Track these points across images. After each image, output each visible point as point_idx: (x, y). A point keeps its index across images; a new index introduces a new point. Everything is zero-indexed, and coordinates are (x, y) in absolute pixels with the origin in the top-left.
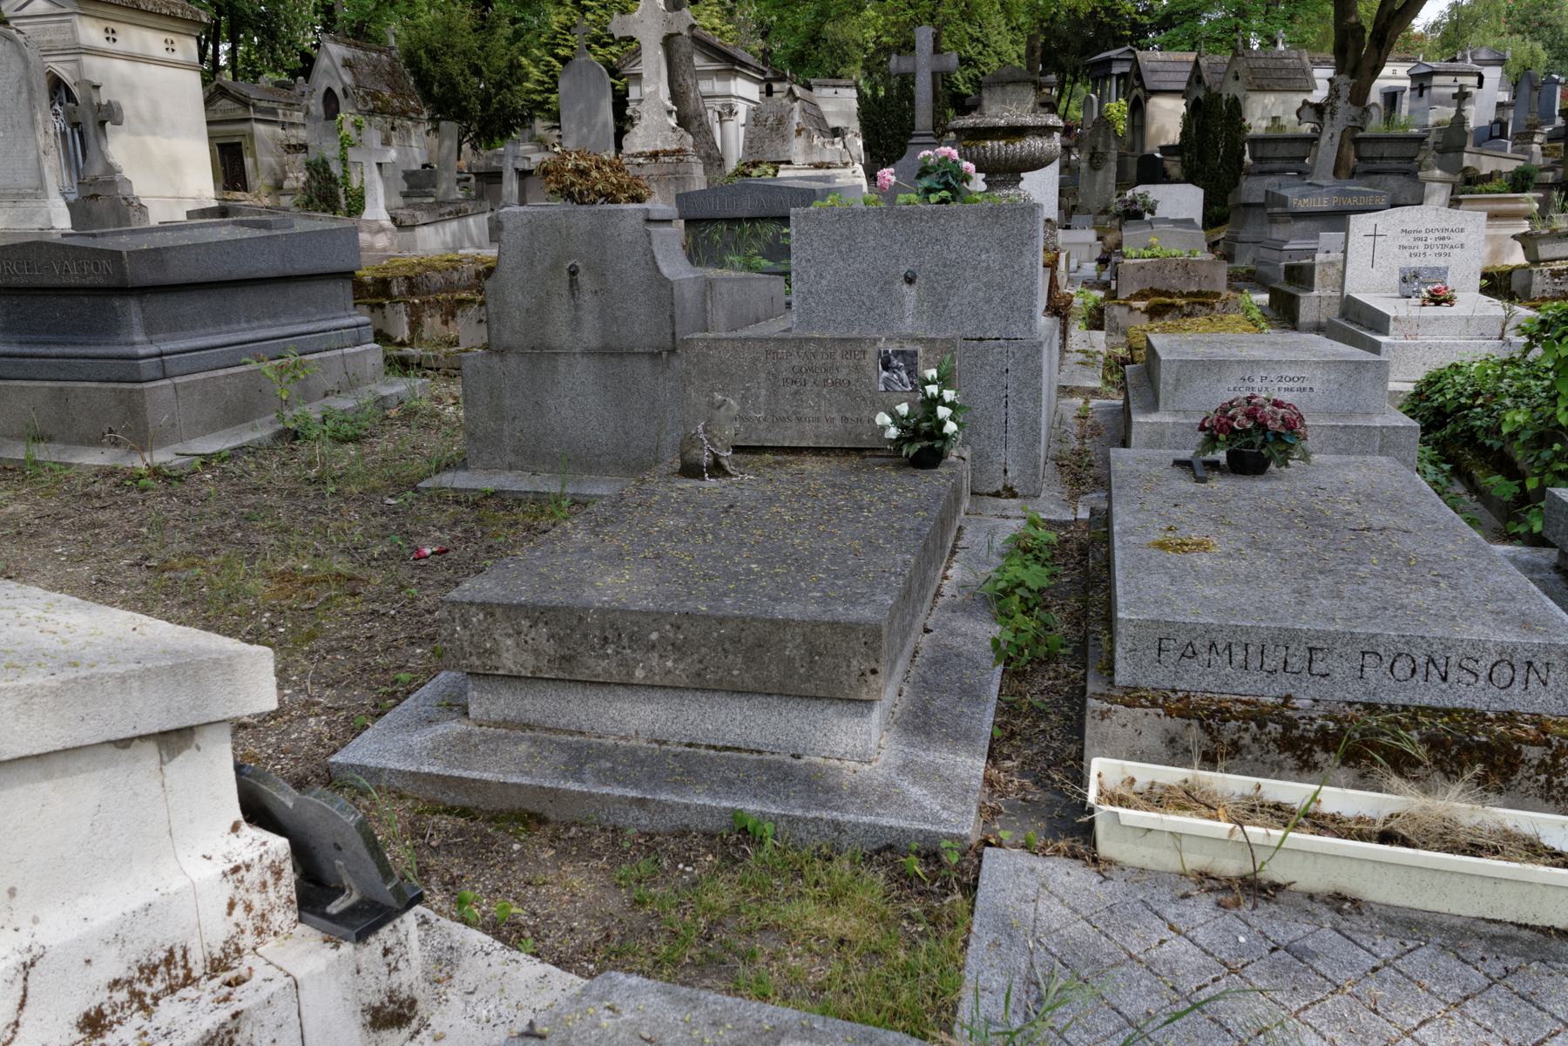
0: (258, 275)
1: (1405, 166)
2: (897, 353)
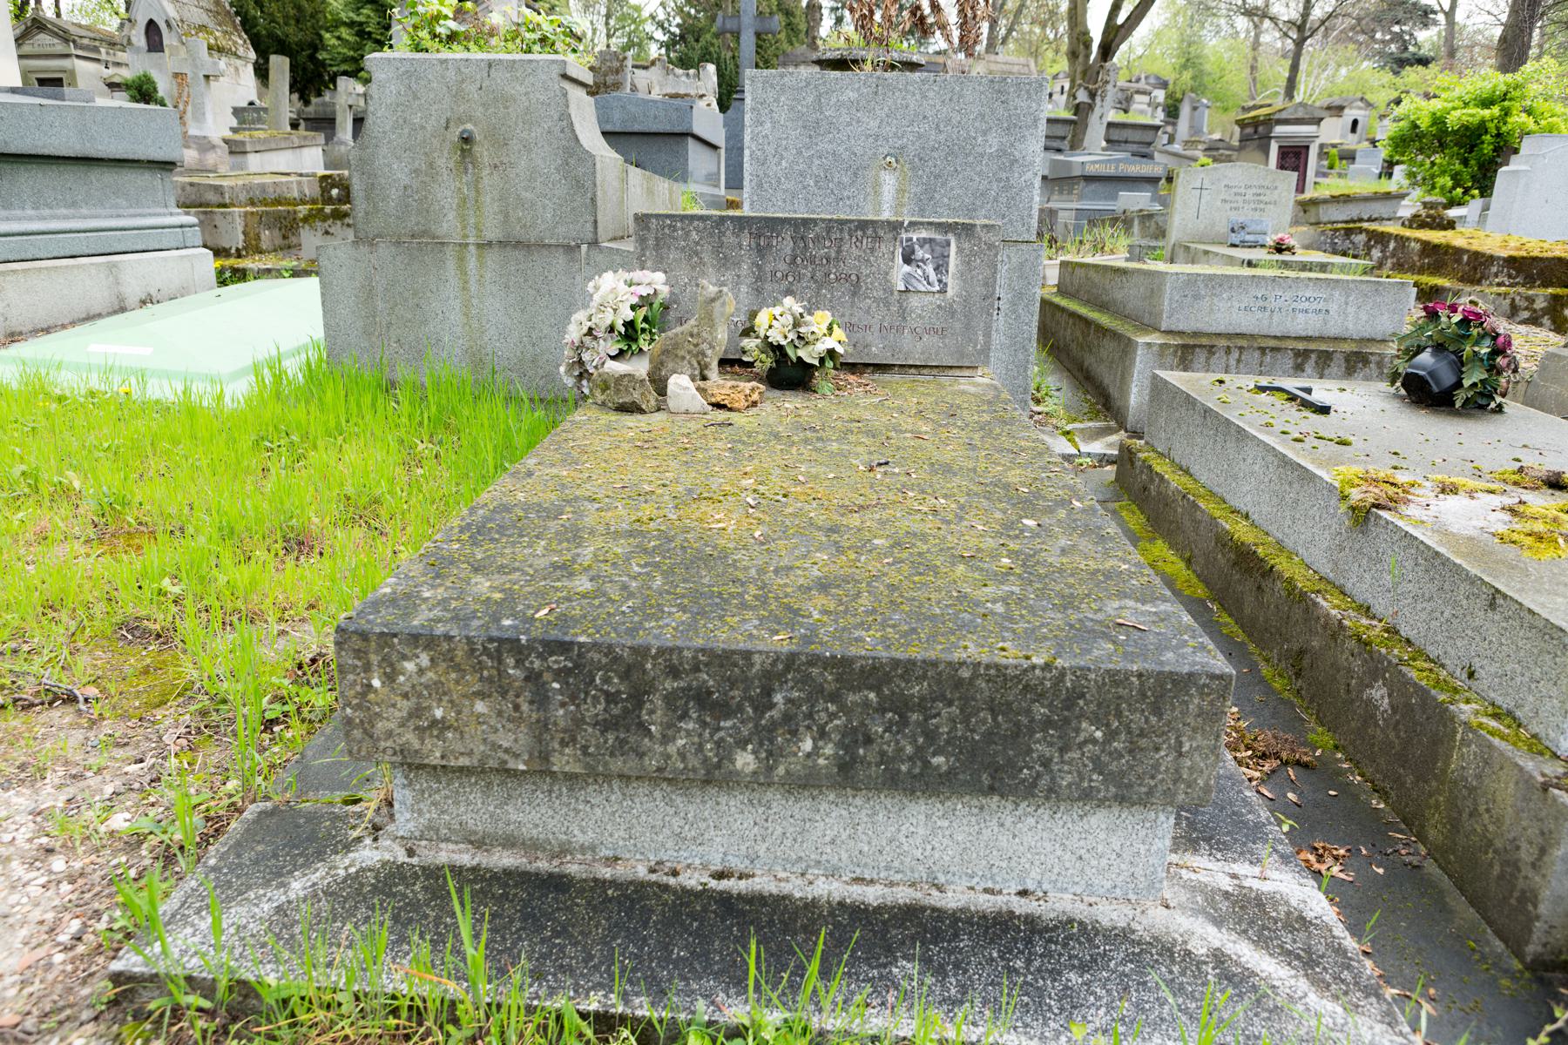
0: (46, 152)
1: (1144, 150)
2: (923, 242)
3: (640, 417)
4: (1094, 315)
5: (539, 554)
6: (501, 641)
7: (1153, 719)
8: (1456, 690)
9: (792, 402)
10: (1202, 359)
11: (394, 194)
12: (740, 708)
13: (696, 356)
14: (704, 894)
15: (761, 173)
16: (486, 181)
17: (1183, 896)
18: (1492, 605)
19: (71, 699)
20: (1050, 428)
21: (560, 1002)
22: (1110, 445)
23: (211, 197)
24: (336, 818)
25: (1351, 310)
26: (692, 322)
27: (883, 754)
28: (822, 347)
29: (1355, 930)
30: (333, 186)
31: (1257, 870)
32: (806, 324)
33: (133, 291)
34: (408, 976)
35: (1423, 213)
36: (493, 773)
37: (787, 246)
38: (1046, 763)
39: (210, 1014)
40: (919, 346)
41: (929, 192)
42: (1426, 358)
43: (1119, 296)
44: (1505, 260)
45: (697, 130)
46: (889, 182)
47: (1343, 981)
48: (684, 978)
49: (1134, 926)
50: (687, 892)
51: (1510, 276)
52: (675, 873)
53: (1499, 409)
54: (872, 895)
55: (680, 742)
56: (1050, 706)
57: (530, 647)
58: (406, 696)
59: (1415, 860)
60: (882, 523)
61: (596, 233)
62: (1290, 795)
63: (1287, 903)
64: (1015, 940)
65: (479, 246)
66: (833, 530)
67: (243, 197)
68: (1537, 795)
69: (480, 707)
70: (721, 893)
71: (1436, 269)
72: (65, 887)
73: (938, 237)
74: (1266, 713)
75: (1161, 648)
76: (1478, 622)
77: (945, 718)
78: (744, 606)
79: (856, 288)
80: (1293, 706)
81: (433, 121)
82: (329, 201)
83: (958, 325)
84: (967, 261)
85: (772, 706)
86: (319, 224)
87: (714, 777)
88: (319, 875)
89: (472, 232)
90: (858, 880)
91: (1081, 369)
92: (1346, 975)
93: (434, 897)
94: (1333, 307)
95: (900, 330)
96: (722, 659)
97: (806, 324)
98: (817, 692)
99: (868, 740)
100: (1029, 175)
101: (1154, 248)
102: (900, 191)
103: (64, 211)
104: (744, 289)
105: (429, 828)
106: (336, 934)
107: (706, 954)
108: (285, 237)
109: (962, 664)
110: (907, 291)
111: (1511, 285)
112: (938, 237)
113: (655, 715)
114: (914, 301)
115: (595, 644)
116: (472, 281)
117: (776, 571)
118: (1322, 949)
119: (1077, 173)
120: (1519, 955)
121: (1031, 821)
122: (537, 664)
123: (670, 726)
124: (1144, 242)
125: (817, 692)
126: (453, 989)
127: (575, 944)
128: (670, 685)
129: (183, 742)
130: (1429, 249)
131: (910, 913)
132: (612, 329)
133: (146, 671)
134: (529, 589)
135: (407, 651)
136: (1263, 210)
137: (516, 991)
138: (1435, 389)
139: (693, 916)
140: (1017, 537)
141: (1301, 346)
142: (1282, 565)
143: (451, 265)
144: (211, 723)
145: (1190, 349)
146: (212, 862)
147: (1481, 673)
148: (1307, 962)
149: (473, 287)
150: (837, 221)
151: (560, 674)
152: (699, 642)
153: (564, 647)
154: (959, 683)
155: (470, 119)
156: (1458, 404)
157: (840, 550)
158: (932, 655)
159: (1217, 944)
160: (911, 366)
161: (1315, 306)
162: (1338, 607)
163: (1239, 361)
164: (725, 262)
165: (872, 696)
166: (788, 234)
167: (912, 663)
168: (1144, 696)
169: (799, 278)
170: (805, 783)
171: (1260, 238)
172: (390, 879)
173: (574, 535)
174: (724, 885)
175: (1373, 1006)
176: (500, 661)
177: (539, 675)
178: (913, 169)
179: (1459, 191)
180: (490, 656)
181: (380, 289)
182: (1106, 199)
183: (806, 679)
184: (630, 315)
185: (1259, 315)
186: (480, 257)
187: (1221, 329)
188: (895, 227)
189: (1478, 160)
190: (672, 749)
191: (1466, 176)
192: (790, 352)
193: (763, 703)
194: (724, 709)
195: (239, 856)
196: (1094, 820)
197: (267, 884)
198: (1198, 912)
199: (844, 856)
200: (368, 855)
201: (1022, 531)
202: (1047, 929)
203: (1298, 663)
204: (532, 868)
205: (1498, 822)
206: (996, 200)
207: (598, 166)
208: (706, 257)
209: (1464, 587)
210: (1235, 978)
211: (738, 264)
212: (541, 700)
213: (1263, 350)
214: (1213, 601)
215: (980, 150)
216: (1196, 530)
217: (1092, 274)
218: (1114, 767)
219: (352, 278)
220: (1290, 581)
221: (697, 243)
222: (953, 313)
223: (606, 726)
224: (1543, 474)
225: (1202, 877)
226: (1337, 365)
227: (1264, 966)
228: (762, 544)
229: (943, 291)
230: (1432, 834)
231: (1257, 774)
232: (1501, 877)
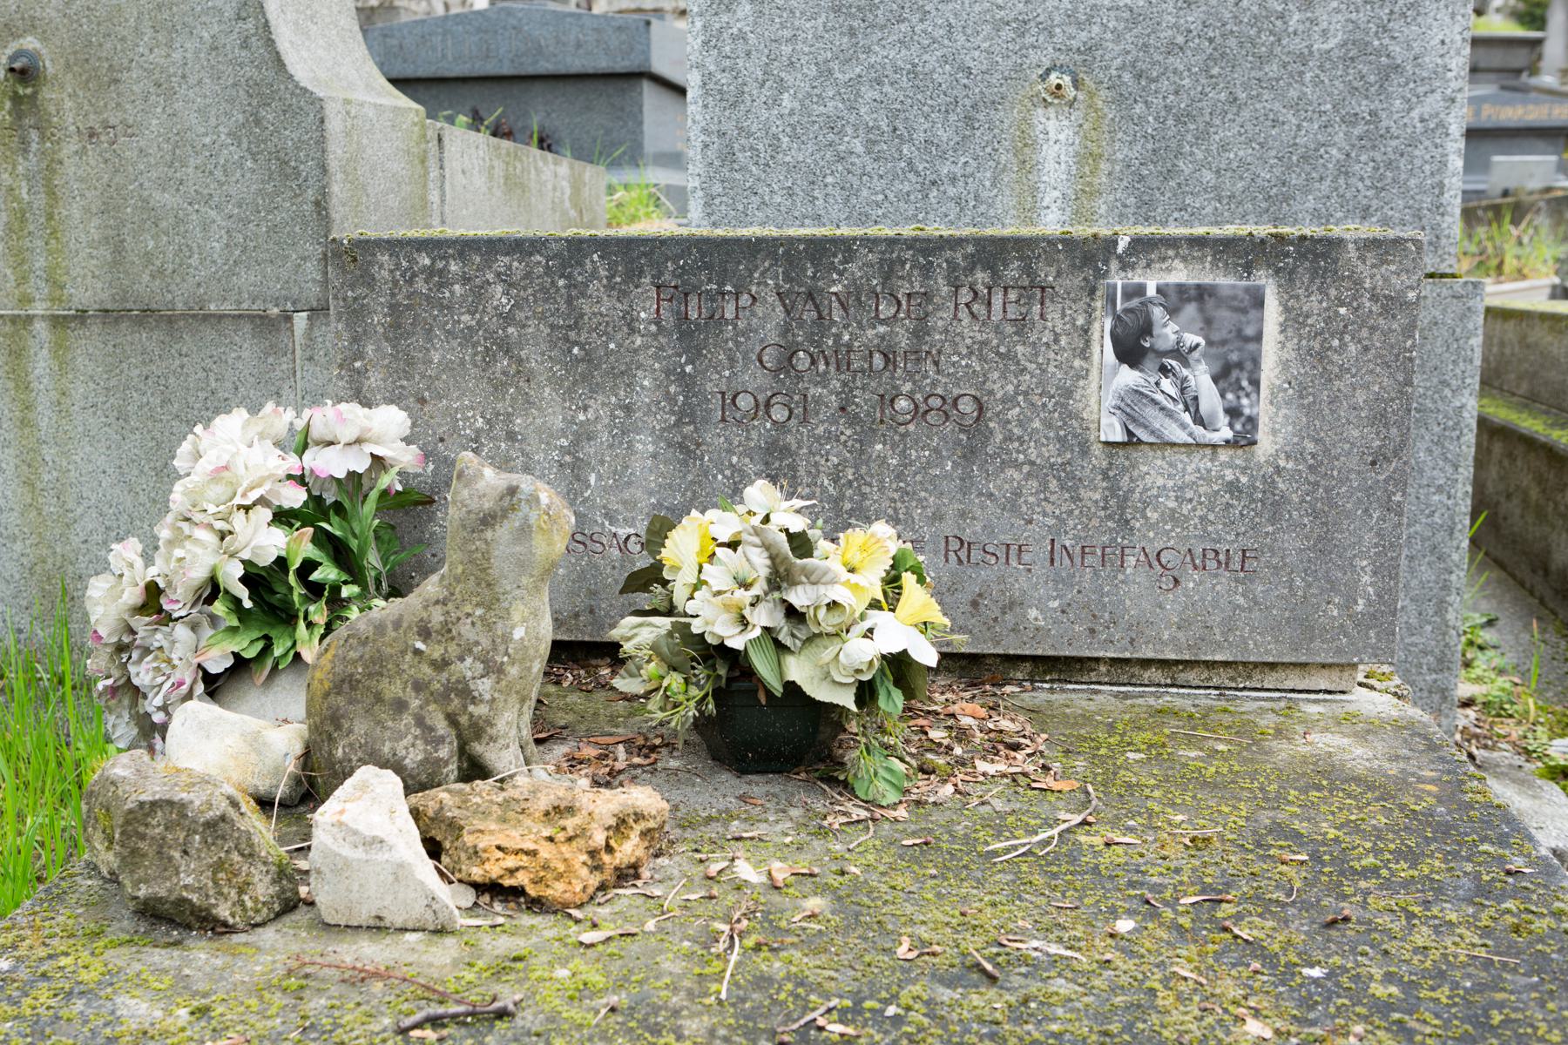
2: (1177, 298)
3: (201, 955)
9: (767, 845)
13: (443, 697)
15: (728, 127)
16: (70, 168)
20: (1504, 755)
26: (431, 587)
28: (861, 652)
32: (814, 578)
37: (768, 320)
40: (1173, 604)
41: (1164, 155)
45: (660, 66)
46: (1057, 136)
65: (57, 322)
73: (1224, 281)
79: (974, 437)
83: (1291, 543)
84: (1316, 355)
89: (38, 287)
95: (1113, 557)
97: (814, 578)
100: (1433, 103)
102: (1087, 158)
104: (644, 444)
110: (1132, 442)
112: (1224, 281)
114: (1153, 473)
132: (212, 590)
149: (45, 418)
150: (911, 243)
155: (32, 27)
160: (1146, 663)
164: (587, 370)
166: (767, 284)
169: (805, 411)
178: (1121, 100)
186: (58, 348)
188: (1089, 255)
192: (762, 665)
206: (1343, 171)
207: (334, 125)
208: (534, 356)
211: (624, 375)
215: (1297, 45)
217: (1539, 334)
221: (508, 319)
222: (1275, 507)
229: (1244, 441)
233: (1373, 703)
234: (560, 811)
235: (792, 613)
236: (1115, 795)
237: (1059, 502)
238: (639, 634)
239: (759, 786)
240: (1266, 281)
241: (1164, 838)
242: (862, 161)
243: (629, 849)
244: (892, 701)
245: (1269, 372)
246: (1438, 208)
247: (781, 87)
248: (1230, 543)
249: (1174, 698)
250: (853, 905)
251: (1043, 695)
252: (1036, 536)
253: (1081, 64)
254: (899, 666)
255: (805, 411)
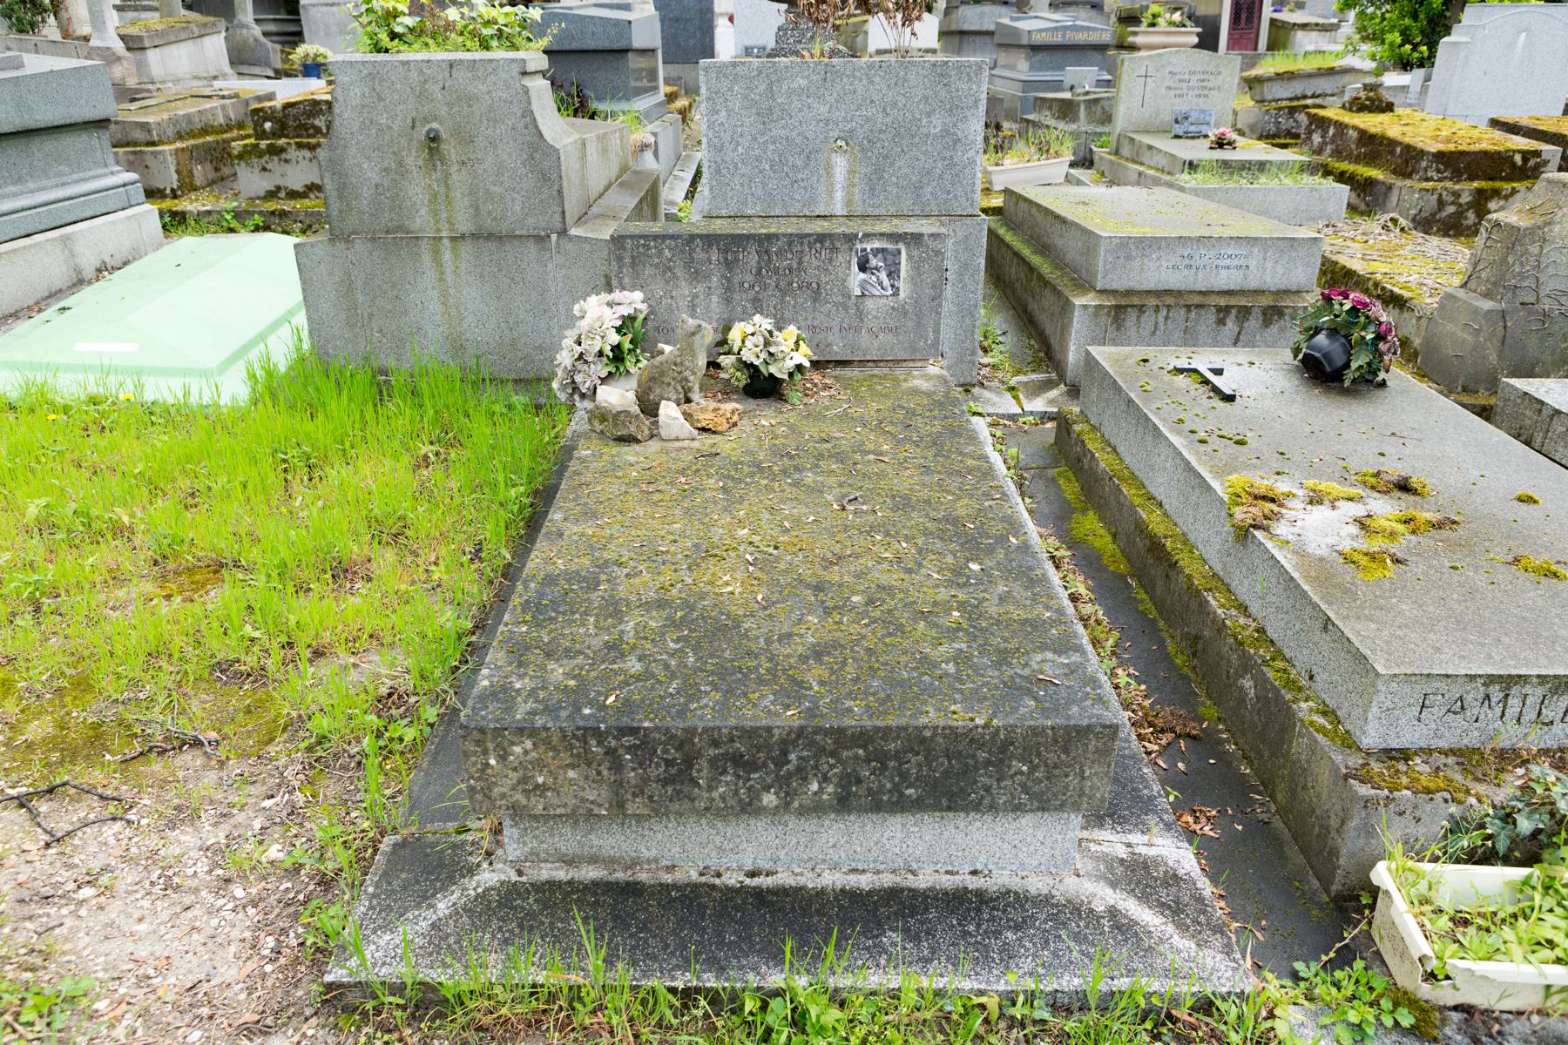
2: (876, 252)
3: (637, 447)
4: (1036, 260)
5: (589, 633)
6: (586, 729)
7: (1063, 757)
8: (1300, 689)
9: (767, 416)
10: (1134, 318)
11: (366, 192)
12: (765, 765)
14: (742, 889)
17: (1090, 866)
18: (1325, 629)
19: (197, 743)
21: (654, 982)
22: (1051, 402)
23: (138, 135)
24: (454, 846)
25: (1269, 264)
27: (869, 789)
28: (790, 364)
29: (1214, 881)
30: (266, 119)
31: (1146, 838)
32: (776, 344)
33: (88, 264)
34: (538, 969)
35: (1363, 95)
36: (582, 817)
37: (753, 259)
38: (988, 789)
39: (404, 1008)
40: (876, 344)
42: (1321, 339)
43: (1059, 242)
44: (1434, 155)
46: (840, 164)
47: (1199, 923)
48: (736, 957)
49: (1054, 892)
50: (729, 889)
51: (1438, 171)
52: (719, 875)
53: (1383, 384)
54: (864, 882)
55: (721, 790)
56: (989, 752)
57: (608, 732)
58: (515, 769)
59: (1264, 817)
60: (858, 576)
61: (564, 222)
62: (1180, 765)
63: (1166, 864)
64: (969, 910)
65: (453, 239)
66: (818, 588)
67: (170, 132)
68: (1341, 782)
69: (571, 774)
70: (754, 888)
71: (1371, 159)
72: (251, 911)
73: (890, 246)
74: (1168, 689)
75: (1070, 702)
76: (1316, 639)
77: (913, 764)
78: (760, 681)
79: (816, 296)
80: (1190, 681)
81: (398, 122)
82: (261, 135)
83: (910, 324)
85: (788, 762)
86: (255, 160)
87: (749, 808)
88: (455, 896)
90: (854, 871)
91: (1025, 311)
92: (1202, 918)
93: (545, 907)
94: (1253, 263)
95: (858, 330)
96: (751, 733)
97: (776, 344)
98: (821, 751)
99: (859, 781)
100: (972, 153)
101: (1100, 134)
102: (851, 172)
103: (12, 189)
104: (715, 299)
105: (532, 854)
106: (480, 942)
107: (749, 937)
108: (217, 170)
109: (925, 727)
110: (863, 295)
111: (1440, 180)
113: (702, 772)
114: (870, 304)
115: (656, 728)
116: (448, 272)
117: (779, 640)
118: (1187, 899)
119: (1025, 42)
120: (1327, 891)
121: (979, 824)
122: (613, 743)
123: (713, 779)
124: (1090, 128)
125: (821, 751)
126: (575, 978)
127: (655, 937)
128: (712, 752)
129: (301, 777)
130: (1366, 138)
131: (893, 893)
132: (601, 354)
133: (248, 711)
134: (593, 674)
135: (515, 739)
136: (1206, 96)
137: (623, 974)
138: (1328, 369)
139: (737, 908)
140: (964, 585)
141: (1222, 302)
142: (1184, 561)
143: (427, 257)
144: (323, 757)
145: (1124, 309)
146: (371, 890)
147: (1317, 678)
148: (1174, 911)
149: (449, 278)
151: (629, 749)
152: (733, 722)
153: (634, 731)
154: (923, 740)
155: (435, 119)
156: (1347, 384)
157: (827, 612)
158: (903, 721)
159: (1112, 902)
161: (1236, 262)
162: (1223, 606)
163: (1167, 318)
164: (696, 276)
165: (860, 751)
166: (753, 248)
167: (889, 728)
168: (1056, 741)
169: (765, 287)
170: (816, 809)
171: (1204, 129)
172: (509, 895)
173: (614, 610)
174: (756, 881)
175: (1218, 941)
176: (586, 743)
177: (616, 750)
178: (863, 150)
179: (1408, 47)
180: (578, 739)
181: (360, 283)
182: (1053, 69)
183: (813, 743)
184: (615, 338)
185: (1186, 272)
186: (454, 249)
187: (1152, 286)
188: (851, 239)
189: (1427, 14)
190: (715, 794)
191: (1415, 31)
192: (763, 369)
193: (782, 761)
194: (752, 766)
195: (390, 884)
196: (1023, 821)
197: (418, 906)
198: (1099, 878)
199: (843, 855)
200: (488, 877)
201: (969, 577)
202: (991, 900)
203: (1195, 644)
204: (612, 878)
205: (1318, 796)
209: (1308, 609)
210: (1123, 927)
211: (708, 277)
212: (617, 766)
213: (1188, 307)
214: (1132, 576)
215: (925, 131)
216: (1120, 510)
218: (1036, 789)
219: (331, 274)
220: (1189, 577)
222: (905, 313)
223: (665, 782)
224: (1394, 478)
225: (1105, 848)
226: (1253, 323)
227: (1144, 917)
228: (765, 608)
229: (896, 294)
230: (1279, 797)
231: (1156, 748)
232: (1319, 836)
233: (933, 370)
234: (715, 410)
235: (771, 354)
236: (858, 399)
237: (842, 314)
238: (726, 361)
239: (761, 402)
240: (901, 246)
241: (872, 408)
242: (769, 173)
243: (735, 418)
244: (798, 377)
245: (903, 273)
246: (973, 191)
247: (738, 144)
248: (892, 324)
249: (876, 371)
250: (793, 429)
251: (838, 372)
252: (835, 324)
253: (848, 138)
254: (799, 367)
255: (765, 287)
